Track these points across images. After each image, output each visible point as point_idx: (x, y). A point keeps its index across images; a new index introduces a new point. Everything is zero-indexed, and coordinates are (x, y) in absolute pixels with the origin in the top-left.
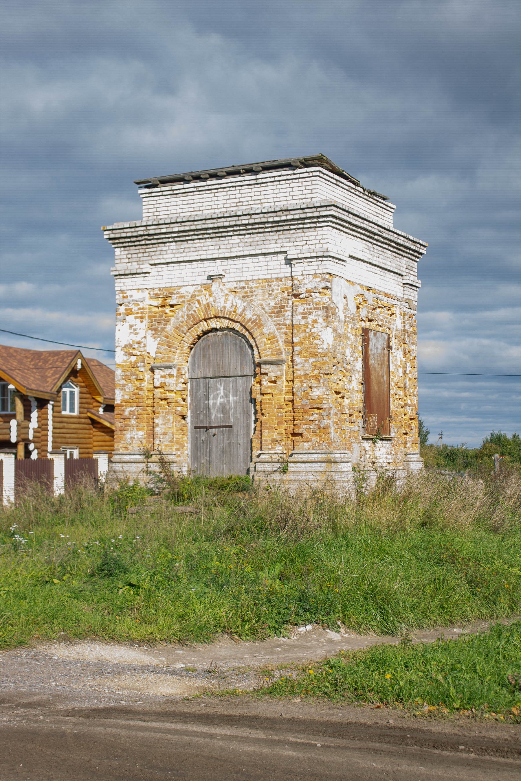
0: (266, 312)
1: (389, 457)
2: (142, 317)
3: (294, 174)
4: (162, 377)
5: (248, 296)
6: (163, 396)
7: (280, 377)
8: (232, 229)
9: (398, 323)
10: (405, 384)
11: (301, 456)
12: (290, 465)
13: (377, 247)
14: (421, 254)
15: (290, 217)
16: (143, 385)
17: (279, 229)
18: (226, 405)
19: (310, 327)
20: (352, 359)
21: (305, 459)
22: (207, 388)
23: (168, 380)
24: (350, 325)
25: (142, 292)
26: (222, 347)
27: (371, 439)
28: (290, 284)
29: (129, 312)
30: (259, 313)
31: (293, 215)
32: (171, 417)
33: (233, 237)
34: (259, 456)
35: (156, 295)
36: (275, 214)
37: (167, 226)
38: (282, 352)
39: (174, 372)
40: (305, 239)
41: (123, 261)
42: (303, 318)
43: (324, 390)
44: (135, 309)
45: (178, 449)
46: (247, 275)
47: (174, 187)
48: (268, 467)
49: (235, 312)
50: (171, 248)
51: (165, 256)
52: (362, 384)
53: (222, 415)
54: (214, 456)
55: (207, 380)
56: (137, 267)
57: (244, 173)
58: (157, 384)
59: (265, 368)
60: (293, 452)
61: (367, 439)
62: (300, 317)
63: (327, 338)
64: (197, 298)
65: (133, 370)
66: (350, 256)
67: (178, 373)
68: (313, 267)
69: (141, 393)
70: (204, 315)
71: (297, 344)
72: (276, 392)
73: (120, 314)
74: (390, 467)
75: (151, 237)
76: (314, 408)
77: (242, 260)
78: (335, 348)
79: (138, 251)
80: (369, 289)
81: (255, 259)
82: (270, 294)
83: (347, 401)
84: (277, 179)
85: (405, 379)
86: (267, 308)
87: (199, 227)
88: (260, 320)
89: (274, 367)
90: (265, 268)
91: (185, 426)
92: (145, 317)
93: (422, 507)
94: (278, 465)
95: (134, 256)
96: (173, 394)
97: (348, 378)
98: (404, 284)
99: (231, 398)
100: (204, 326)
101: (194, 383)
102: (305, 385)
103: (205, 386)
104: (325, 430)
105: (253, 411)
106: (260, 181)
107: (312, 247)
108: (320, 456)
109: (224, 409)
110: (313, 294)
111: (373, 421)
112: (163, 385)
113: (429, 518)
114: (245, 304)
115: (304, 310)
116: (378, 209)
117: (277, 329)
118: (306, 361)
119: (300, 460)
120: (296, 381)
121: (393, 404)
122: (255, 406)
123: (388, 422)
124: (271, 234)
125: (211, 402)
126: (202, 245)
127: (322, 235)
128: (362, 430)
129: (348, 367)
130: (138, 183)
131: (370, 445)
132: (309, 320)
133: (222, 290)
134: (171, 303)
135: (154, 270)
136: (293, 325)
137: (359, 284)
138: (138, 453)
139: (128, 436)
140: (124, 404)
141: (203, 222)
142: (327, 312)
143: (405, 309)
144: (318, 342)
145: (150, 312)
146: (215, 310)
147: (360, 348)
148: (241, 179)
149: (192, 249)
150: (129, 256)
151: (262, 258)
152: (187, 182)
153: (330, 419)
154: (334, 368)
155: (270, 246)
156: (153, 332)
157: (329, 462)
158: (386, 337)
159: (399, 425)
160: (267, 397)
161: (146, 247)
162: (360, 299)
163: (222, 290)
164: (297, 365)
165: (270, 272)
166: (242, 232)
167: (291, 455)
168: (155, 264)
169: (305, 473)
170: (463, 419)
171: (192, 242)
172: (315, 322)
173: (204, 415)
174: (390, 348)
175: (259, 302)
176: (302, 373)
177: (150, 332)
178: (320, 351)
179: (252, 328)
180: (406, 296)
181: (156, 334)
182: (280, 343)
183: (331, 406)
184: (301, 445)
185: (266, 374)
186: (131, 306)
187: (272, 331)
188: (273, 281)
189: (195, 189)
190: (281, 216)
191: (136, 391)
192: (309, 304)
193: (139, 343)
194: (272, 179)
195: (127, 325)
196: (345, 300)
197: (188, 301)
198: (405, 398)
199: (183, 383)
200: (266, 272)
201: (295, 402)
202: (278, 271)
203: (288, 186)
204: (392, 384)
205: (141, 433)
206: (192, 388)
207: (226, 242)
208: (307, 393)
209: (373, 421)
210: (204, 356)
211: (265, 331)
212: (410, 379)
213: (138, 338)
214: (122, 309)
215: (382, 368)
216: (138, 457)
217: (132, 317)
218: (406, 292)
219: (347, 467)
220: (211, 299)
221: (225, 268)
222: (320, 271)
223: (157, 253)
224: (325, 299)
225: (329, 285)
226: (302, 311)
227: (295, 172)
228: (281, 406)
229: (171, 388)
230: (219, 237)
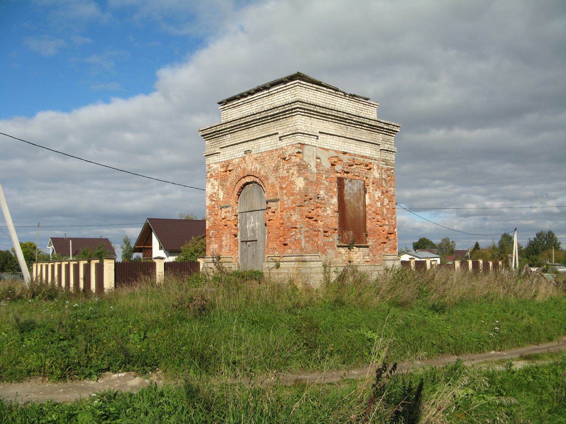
2: (216, 179)
3: (286, 86)
6: (225, 224)
7: (276, 210)
14: (397, 132)
15: (278, 112)
27: (348, 246)
29: (211, 176)
30: (267, 171)
32: (228, 236)
35: (223, 165)
40: (287, 124)
44: (214, 174)
46: (263, 149)
47: (234, 103)
58: (223, 217)
61: (342, 247)
66: (320, 132)
67: (233, 210)
69: (216, 222)
77: (260, 140)
80: (345, 153)
87: (238, 124)
89: (274, 204)
91: (237, 241)
100: (244, 181)
106: (271, 93)
107: (291, 128)
108: (296, 257)
109: (253, 230)
116: (361, 106)
118: (289, 199)
125: (248, 226)
130: (220, 103)
135: (222, 151)
139: (211, 247)
144: (294, 186)
147: (336, 190)
148: (262, 93)
151: (268, 138)
152: (239, 99)
158: (362, 183)
160: (271, 222)
177: (220, 187)
180: (382, 157)
185: (270, 208)
193: (215, 193)
195: (210, 184)
205: (217, 245)
211: (270, 182)
213: (215, 191)
214: (209, 174)
217: (212, 179)
224: (298, 160)
225: (300, 150)
230: (248, 128)
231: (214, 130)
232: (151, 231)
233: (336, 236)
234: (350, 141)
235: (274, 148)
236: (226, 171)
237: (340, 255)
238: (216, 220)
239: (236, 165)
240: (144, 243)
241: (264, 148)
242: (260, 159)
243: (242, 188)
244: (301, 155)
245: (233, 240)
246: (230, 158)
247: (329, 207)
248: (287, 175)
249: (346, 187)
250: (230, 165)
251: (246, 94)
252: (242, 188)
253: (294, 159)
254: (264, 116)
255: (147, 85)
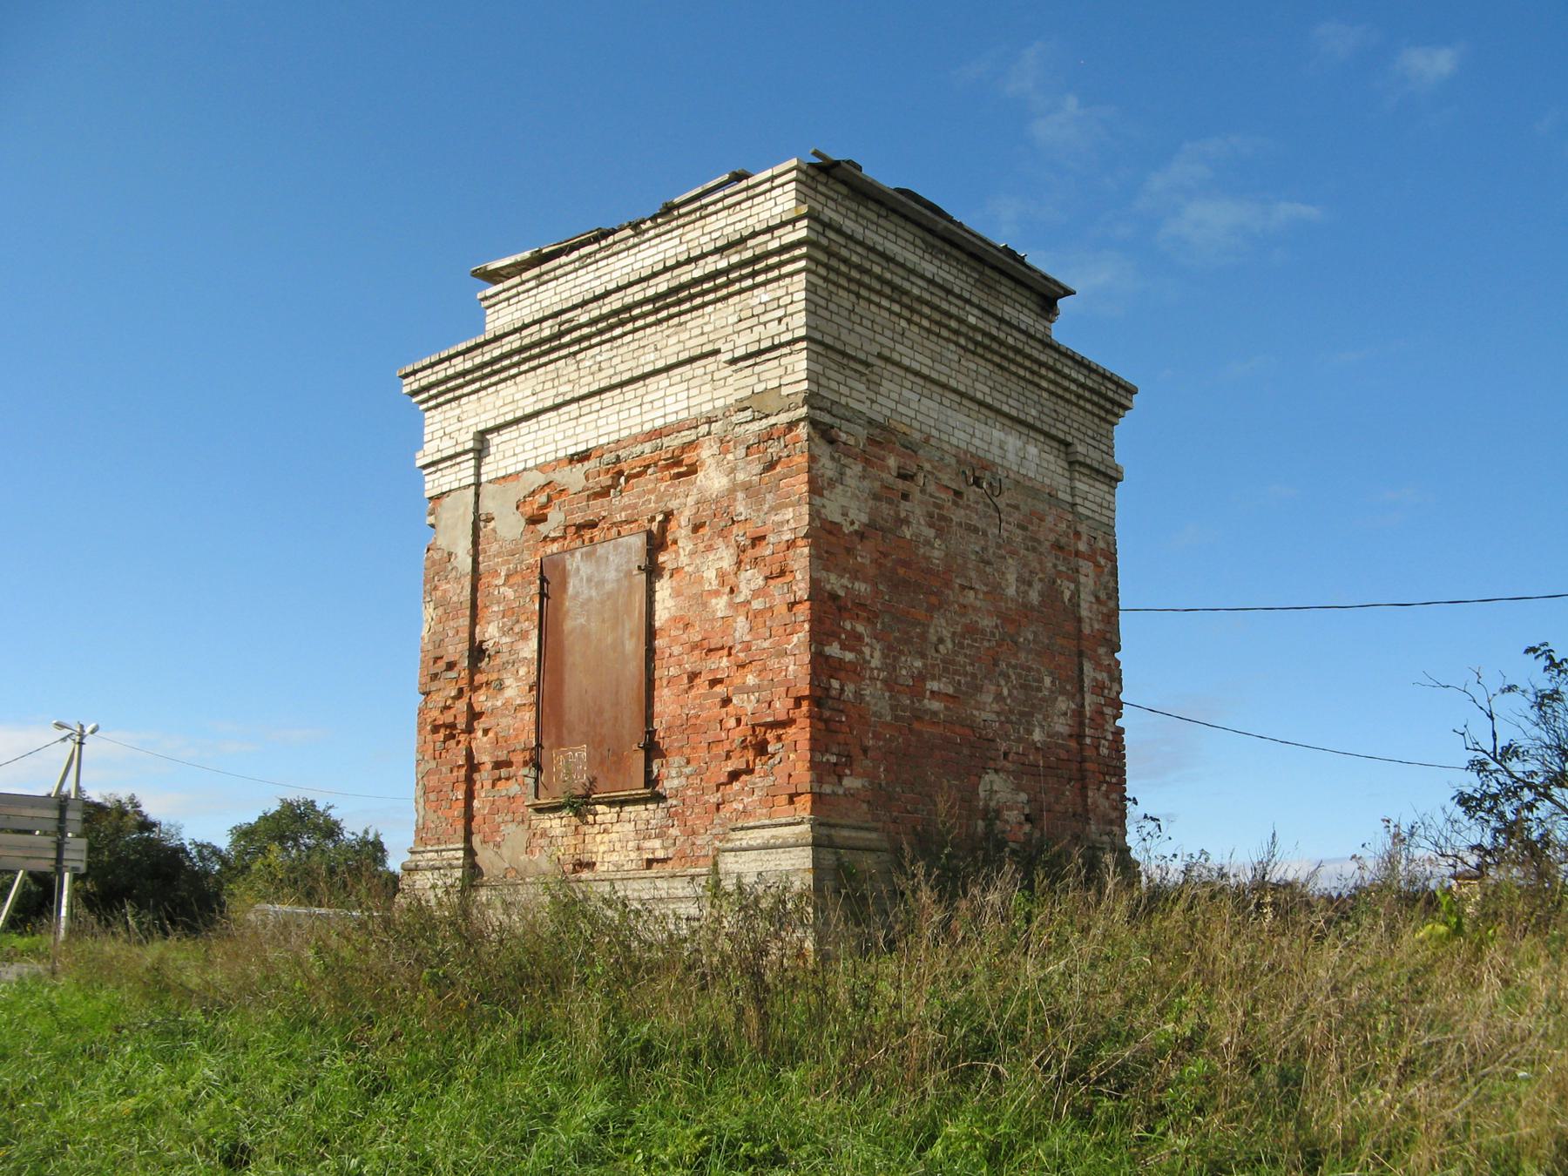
237: (543, 842)
249: (573, 585)
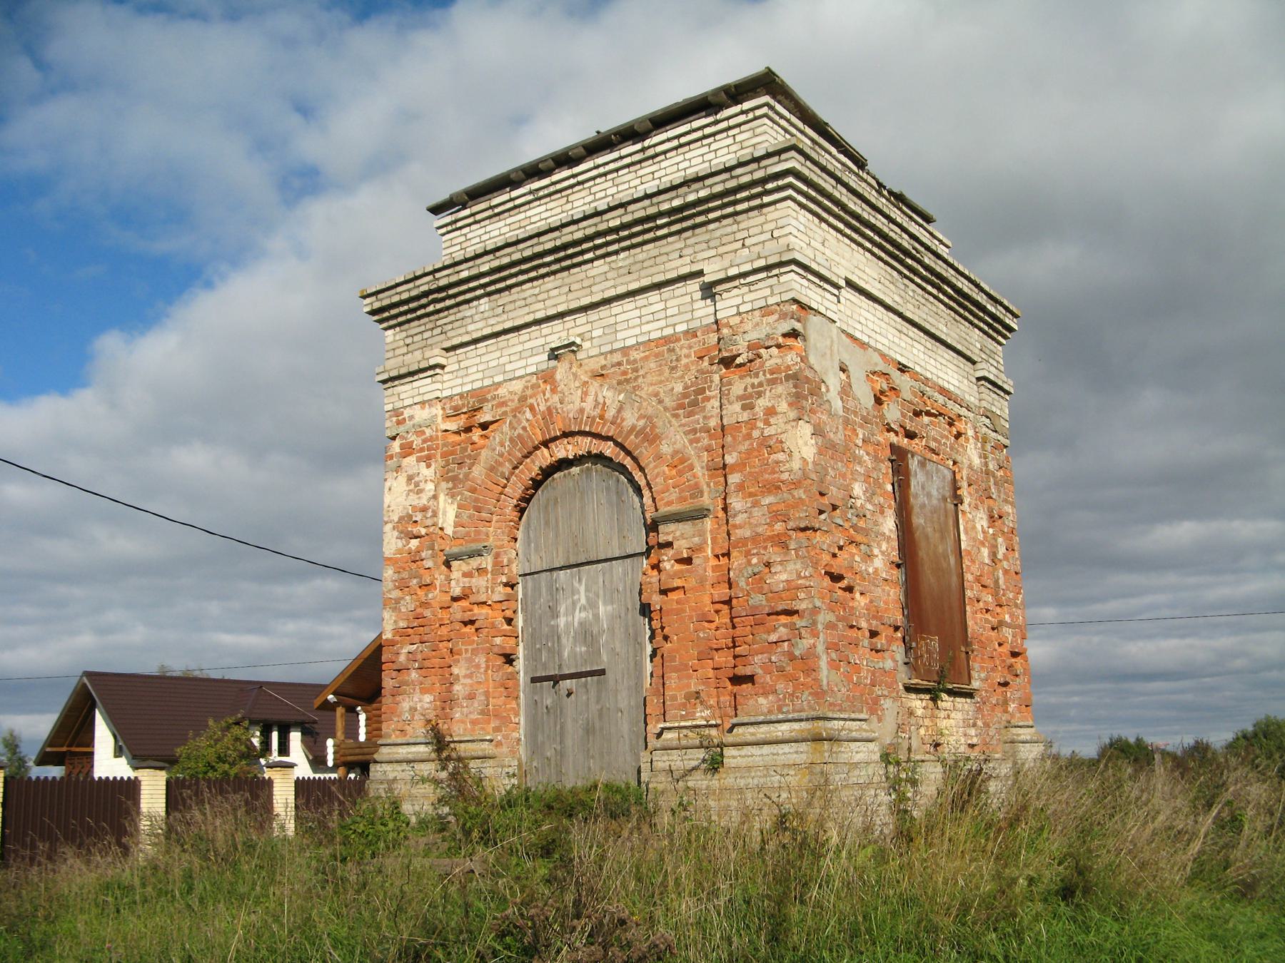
0: (666, 409)
1: (972, 732)
2: (429, 458)
3: (716, 122)
4: (465, 575)
5: (627, 381)
6: (467, 616)
7: (699, 549)
8: (591, 244)
9: (972, 455)
10: (997, 582)
11: (751, 729)
12: (728, 752)
13: (913, 286)
14: (1010, 330)
15: (703, 194)
16: (430, 596)
17: (685, 224)
18: (591, 625)
19: (760, 424)
20: (869, 506)
21: (760, 737)
22: (554, 591)
23: (479, 582)
24: (860, 432)
25: (430, 406)
26: (582, 499)
28: (714, 338)
29: (407, 450)
30: (650, 411)
31: (711, 186)
32: (481, 660)
33: (596, 263)
34: (659, 735)
35: (456, 408)
36: (673, 194)
37: (471, 264)
38: (702, 493)
39: (487, 562)
40: (739, 236)
41: (398, 352)
42: (744, 408)
43: (799, 566)
44: (417, 442)
45: (497, 729)
46: (628, 337)
47: (495, 201)
48: (677, 761)
49: (602, 417)
50: (482, 308)
51: (470, 328)
52: (898, 566)
53: (584, 649)
54: (569, 742)
55: (555, 574)
56: (420, 358)
57: (621, 143)
58: (457, 591)
59: (668, 532)
60: (735, 721)
62: (737, 407)
63: (802, 444)
64: (530, 401)
65: (414, 566)
66: (849, 283)
67: (495, 564)
68: (763, 292)
69: (427, 613)
70: (543, 434)
71: (735, 468)
72: (692, 583)
73: (391, 457)
74: (974, 754)
75: (444, 294)
76: (778, 613)
77: (616, 308)
78: (822, 472)
79: (423, 328)
80: (903, 369)
81: (640, 300)
82: (673, 369)
83: (860, 601)
84: (683, 140)
85: (995, 570)
86: (667, 400)
87: (528, 253)
88: (654, 427)
89: (686, 527)
90: (662, 315)
91: (513, 677)
92: (435, 456)
93: (1055, 844)
94: (701, 754)
95: (416, 338)
96: (485, 610)
97: (862, 547)
98: (979, 379)
99: (602, 609)
100: (544, 458)
101: (530, 584)
102: (755, 561)
103: (550, 588)
104: (807, 663)
105: (648, 633)
106: (650, 152)
107: (756, 249)
108: (796, 726)
109: (587, 634)
110: (762, 351)
111: (928, 651)
112: (467, 591)
113: (1080, 873)
114: (621, 397)
115: (746, 389)
117: (691, 442)
119: (750, 738)
120: (734, 554)
121: (974, 618)
122: (651, 620)
123: (963, 655)
124: (670, 239)
125: (562, 621)
126: (537, 291)
127: (776, 220)
128: (902, 668)
129: (861, 524)
130: (436, 210)
131: (924, 704)
132: (757, 409)
133: (575, 375)
134: (482, 421)
135: (451, 361)
136: (723, 426)
137: (876, 350)
138: (423, 740)
139: (406, 705)
140: (397, 638)
141: (535, 241)
142: (795, 387)
143: (985, 429)
144: (781, 456)
145: (444, 445)
146: (564, 419)
147: (889, 488)
148: (615, 155)
149: (518, 304)
150: (409, 341)
151: (654, 296)
153: (816, 636)
154: (823, 517)
155: (668, 266)
156: (450, 485)
157: (817, 739)
159: (989, 665)
160: (672, 596)
161: (436, 317)
162: (882, 384)
163: (575, 375)
164: (735, 516)
165: (670, 321)
166: (611, 248)
167: (731, 730)
168: (454, 348)
169: (765, 768)
170: (1074, 727)
171: (518, 289)
172: (771, 412)
173: (549, 650)
174: (958, 500)
175: (651, 389)
176: (748, 533)
177: (444, 485)
178: (785, 476)
179: (637, 447)
180: (984, 404)
181: (454, 487)
182: (698, 470)
183: (818, 603)
184: (751, 702)
185: (669, 545)
186: (411, 437)
187: (678, 446)
188: (678, 340)
189: (531, 197)
190: (686, 194)
191: (419, 610)
192: (757, 375)
193: (424, 509)
194: (675, 143)
195: (402, 479)
196: (843, 376)
197: (513, 411)
198: (998, 610)
199: (506, 585)
200: (663, 323)
201: (734, 602)
202: (688, 316)
203: (705, 149)
204: (968, 577)
205: (428, 698)
206: (525, 595)
207: (582, 275)
208: (761, 579)
209: (928, 651)
210: (547, 523)
211: (666, 449)
212: (1006, 572)
213: (424, 501)
214: (396, 446)
215: (943, 538)
216: (422, 748)
217: (411, 460)
218: (984, 396)
219: (866, 753)
220: (556, 398)
221: (579, 330)
222: (776, 299)
223: (457, 324)
224: (791, 358)
225: (798, 326)
226: (741, 392)
227: (719, 117)
228: (704, 615)
229: (483, 598)
230: (568, 268)
231: (424, 285)
232: (93, 706)
233: (898, 651)
234: (914, 332)
235: (681, 328)
236: (468, 430)
238: (425, 604)
239: (512, 405)
240: (71, 739)
241: (637, 331)
242: (621, 371)
243: (537, 484)
244: (798, 344)
245: (498, 676)
246: (487, 382)
247: (879, 546)
248: (745, 416)
250: (487, 407)
251: (551, 163)
252: (537, 484)
253: (772, 358)
254: (639, 215)
255: (66, 371)
